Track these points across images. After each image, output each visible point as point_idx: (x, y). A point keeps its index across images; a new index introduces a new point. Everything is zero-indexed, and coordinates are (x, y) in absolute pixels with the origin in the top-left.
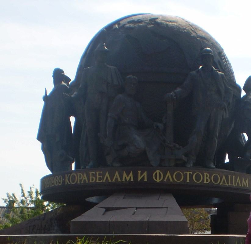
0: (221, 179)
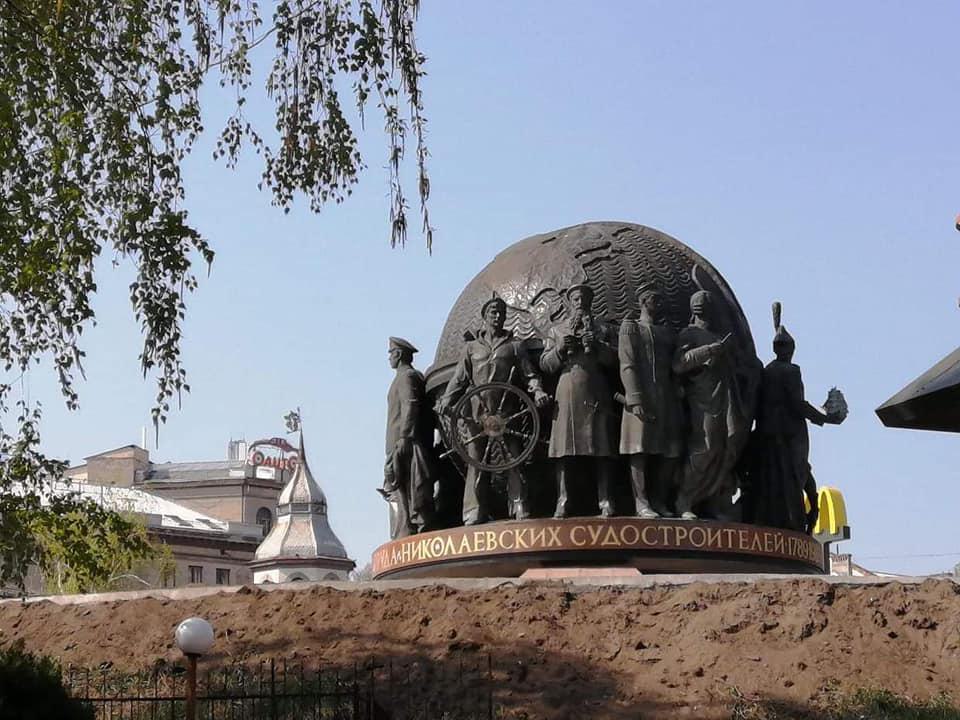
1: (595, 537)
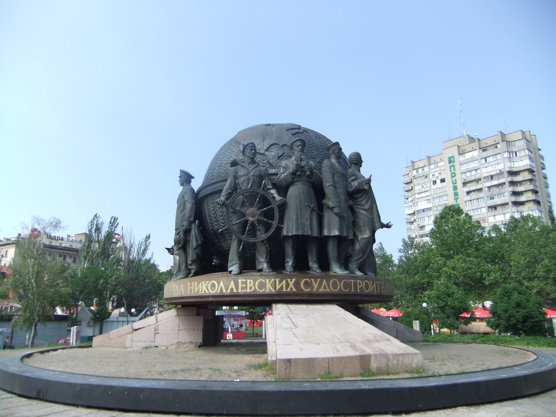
0: (219, 286)
1: (316, 286)
